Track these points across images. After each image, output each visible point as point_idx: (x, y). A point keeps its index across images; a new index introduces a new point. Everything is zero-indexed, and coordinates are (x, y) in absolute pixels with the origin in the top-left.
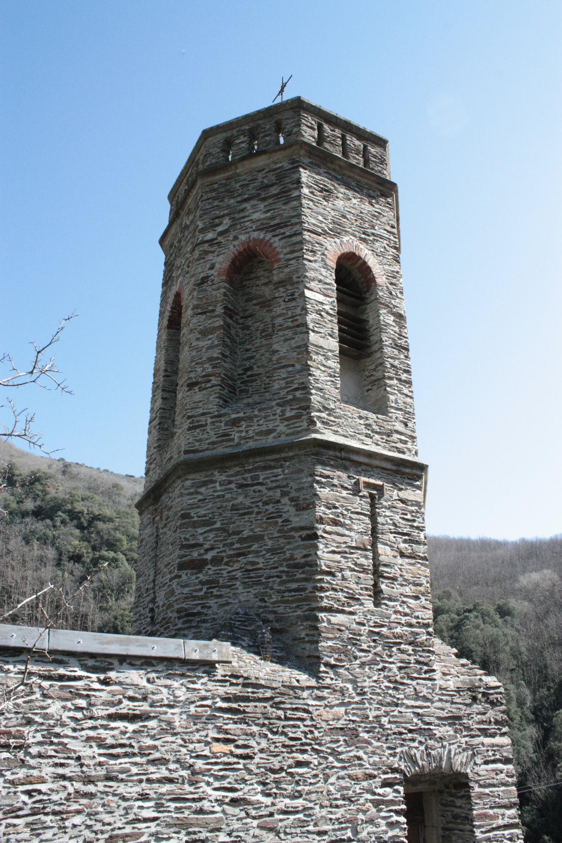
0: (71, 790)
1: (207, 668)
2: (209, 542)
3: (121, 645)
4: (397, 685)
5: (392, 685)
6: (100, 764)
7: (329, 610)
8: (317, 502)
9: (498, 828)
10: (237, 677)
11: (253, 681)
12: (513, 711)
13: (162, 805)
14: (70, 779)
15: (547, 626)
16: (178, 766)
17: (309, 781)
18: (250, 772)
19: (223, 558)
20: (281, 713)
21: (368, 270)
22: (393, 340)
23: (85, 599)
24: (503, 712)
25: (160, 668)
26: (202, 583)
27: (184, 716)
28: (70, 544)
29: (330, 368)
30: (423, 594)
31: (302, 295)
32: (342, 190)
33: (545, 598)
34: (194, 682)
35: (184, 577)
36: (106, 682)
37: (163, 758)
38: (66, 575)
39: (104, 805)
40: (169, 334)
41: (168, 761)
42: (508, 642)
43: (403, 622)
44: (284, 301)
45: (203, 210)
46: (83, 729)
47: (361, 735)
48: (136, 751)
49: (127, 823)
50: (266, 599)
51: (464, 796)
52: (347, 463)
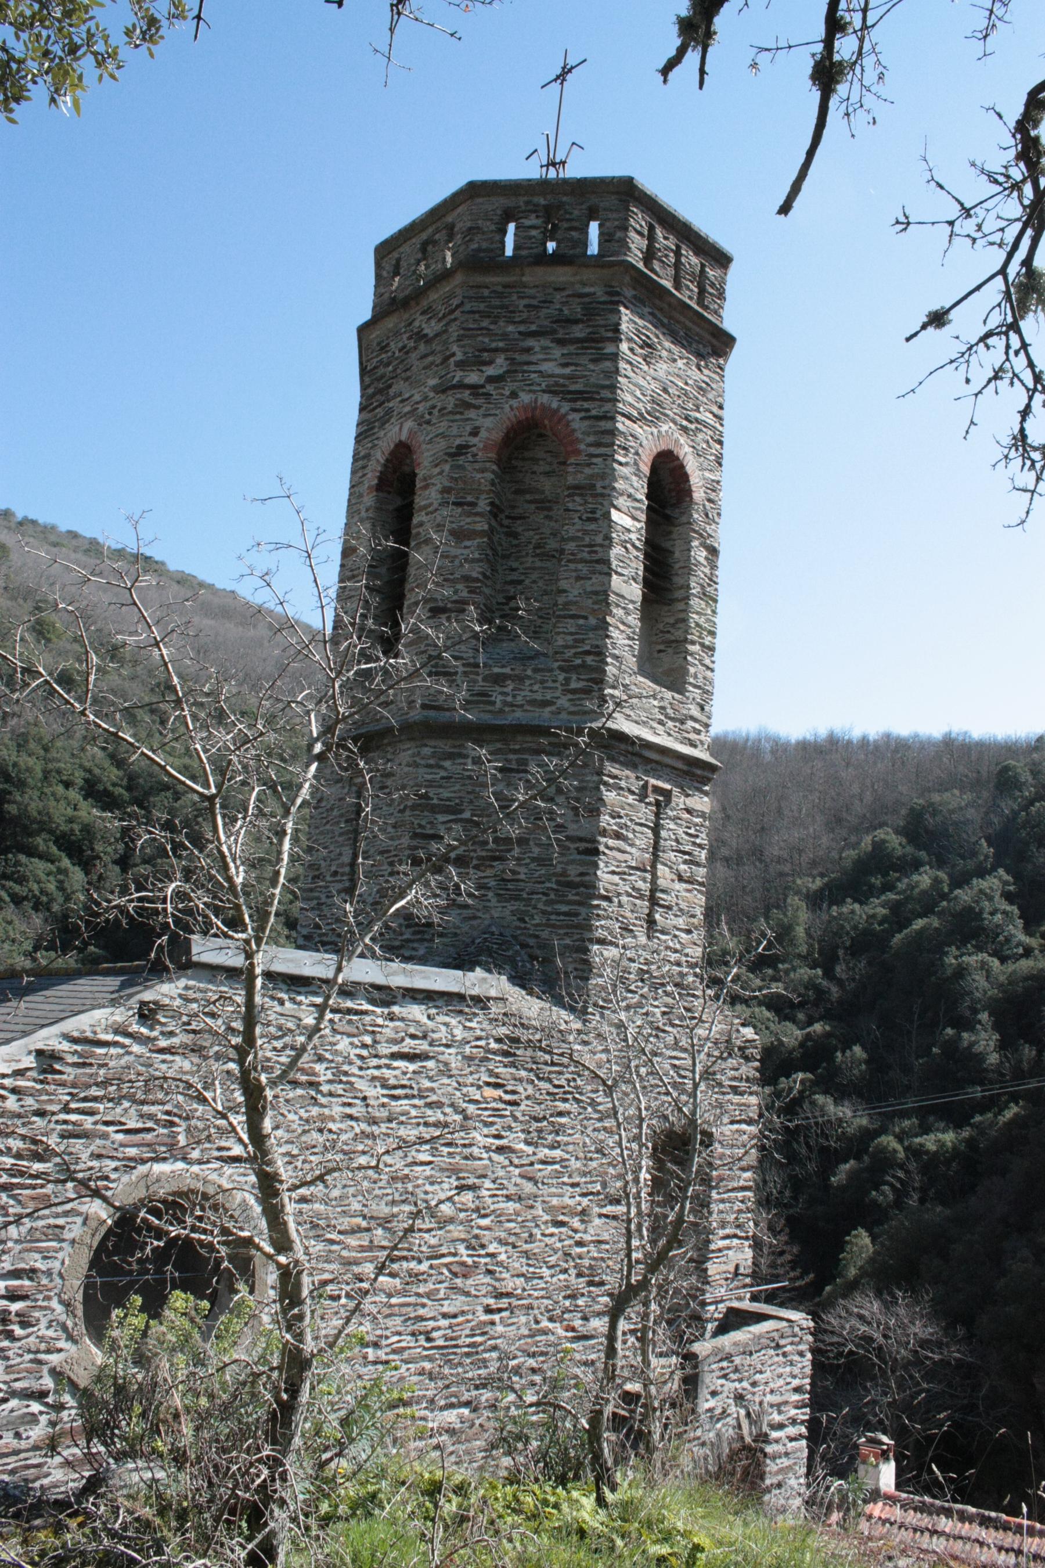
6: (383, 1105)
7: (602, 942)
8: (602, 809)
13: (437, 1149)
14: (357, 1119)
18: (515, 1119)
20: (547, 1057)
21: (685, 477)
22: (703, 587)
25: (439, 1003)
27: (459, 1057)
29: (629, 627)
30: (696, 928)
31: (607, 515)
32: (667, 344)
34: (470, 1020)
36: (392, 1017)
40: (379, 501)
44: (580, 518)
45: (464, 329)
48: (416, 1092)
49: (406, 1166)
52: (636, 759)
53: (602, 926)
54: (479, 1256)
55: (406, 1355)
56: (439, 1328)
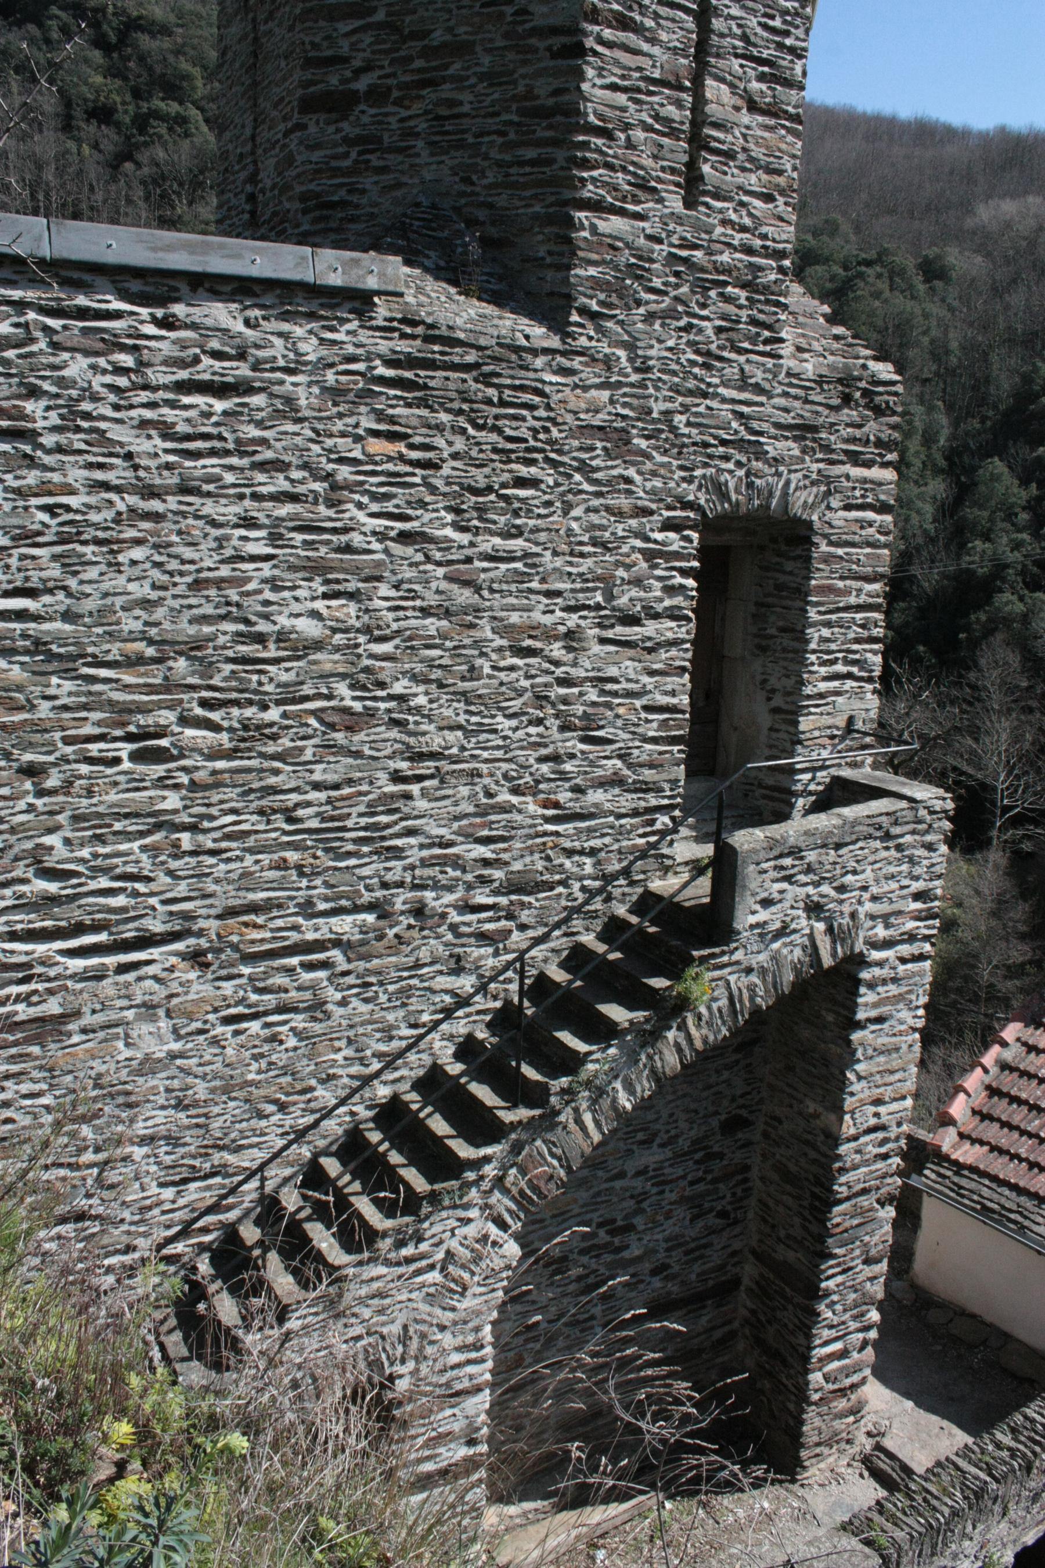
0: (121, 507)
1: (357, 304)
2: (361, 55)
3: (192, 253)
4: (710, 359)
5: (700, 359)
6: (168, 466)
7: (597, 206)
9: (847, 609)
10: (413, 323)
11: (444, 332)
12: (912, 451)
13: (281, 536)
15: (1007, 307)
16: (306, 474)
17: (537, 511)
18: (433, 490)
19: (389, 89)
20: (492, 392)
23: (129, 201)
24: (894, 427)
26: (347, 141)
27: (316, 390)
28: (86, 84)
30: (782, 192)
33: (1017, 252)
34: (332, 329)
35: (312, 129)
36: (167, 323)
37: (278, 460)
38: (86, 150)
39: (180, 533)
41: (289, 465)
42: (929, 329)
43: (736, 242)
46: (132, 407)
47: (635, 441)
48: (231, 446)
49: (222, 562)
50: (474, 178)
51: (800, 557)
53: (594, 180)
54: (375, 699)
55: (251, 842)
56: (308, 804)
